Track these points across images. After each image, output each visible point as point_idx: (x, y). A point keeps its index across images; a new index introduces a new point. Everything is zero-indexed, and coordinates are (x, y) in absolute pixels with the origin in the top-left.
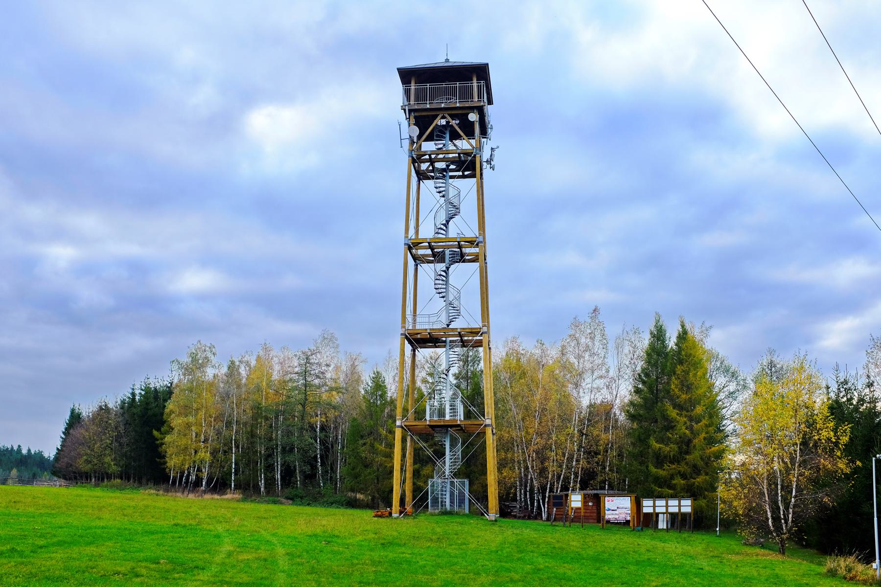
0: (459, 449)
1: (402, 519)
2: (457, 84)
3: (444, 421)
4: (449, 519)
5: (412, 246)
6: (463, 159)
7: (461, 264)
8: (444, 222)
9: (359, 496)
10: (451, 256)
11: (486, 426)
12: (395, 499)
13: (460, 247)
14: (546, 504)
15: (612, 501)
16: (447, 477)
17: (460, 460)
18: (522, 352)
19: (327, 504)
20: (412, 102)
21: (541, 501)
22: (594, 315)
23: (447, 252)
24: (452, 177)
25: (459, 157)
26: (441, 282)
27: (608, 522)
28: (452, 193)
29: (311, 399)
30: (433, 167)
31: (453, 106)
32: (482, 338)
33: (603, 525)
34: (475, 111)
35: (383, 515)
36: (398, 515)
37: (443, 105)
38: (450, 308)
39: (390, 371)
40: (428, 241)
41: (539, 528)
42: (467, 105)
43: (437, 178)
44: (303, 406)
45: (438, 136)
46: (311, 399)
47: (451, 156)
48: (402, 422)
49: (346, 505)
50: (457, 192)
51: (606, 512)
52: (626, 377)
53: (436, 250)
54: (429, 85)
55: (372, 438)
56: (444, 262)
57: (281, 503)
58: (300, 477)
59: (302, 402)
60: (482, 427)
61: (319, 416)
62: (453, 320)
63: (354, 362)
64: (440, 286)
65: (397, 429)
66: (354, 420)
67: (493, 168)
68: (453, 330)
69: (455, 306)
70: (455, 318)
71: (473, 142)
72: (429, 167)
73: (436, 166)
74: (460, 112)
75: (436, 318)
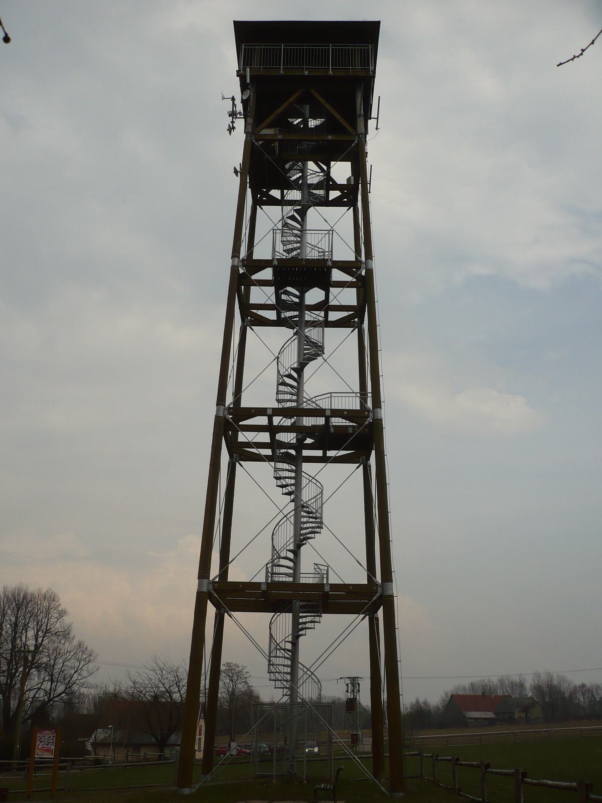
8: (291, 547)
26: (288, 397)
38: (303, 514)
62: (307, 625)
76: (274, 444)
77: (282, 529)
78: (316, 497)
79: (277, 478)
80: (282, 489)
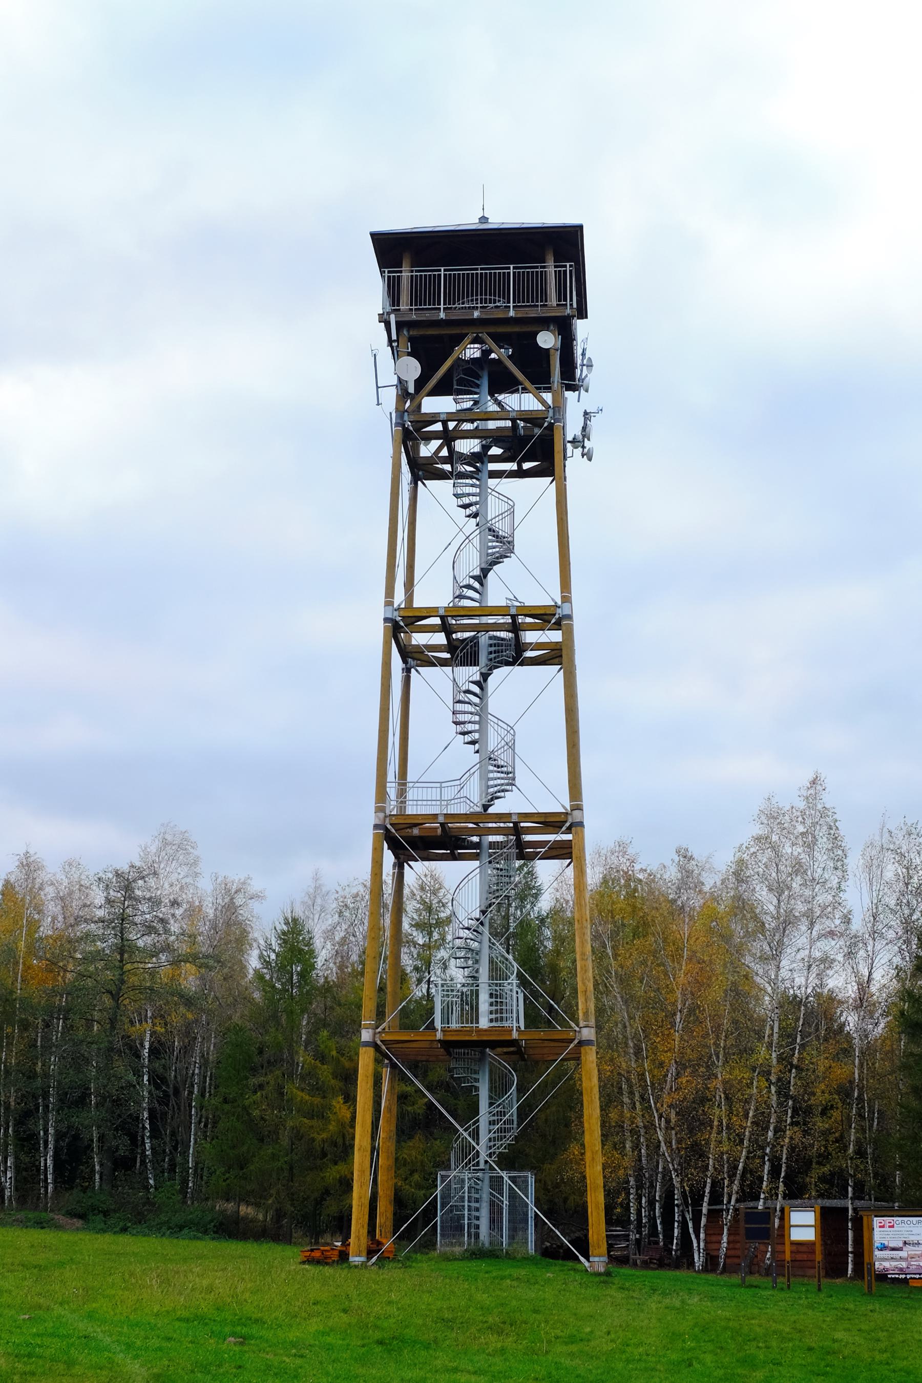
0: (512, 1102)
1: (375, 1268)
2: (509, 268)
3: (479, 1031)
4: (490, 1268)
5: (402, 624)
6: (522, 432)
7: (517, 669)
8: (477, 572)
9: (245, 1210)
10: (493, 649)
11: (581, 1043)
12: (358, 1219)
13: (515, 628)
14: (702, 1231)
15: (890, 1227)
16: (482, 1166)
17: (515, 1126)
18: (641, 876)
19: (169, 1228)
20: (404, 307)
21: (690, 1225)
22: (812, 791)
23: (484, 639)
24: (494, 474)
25: (515, 426)
27: (882, 1277)
28: (494, 507)
29: (133, 980)
30: (451, 450)
31: (501, 316)
32: (569, 837)
33: (870, 1287)
34: (552, 327)
35: (326, 1258)
36: (363, 1259)
37: (476, 314)
38: (491, 768)
39: (316, 920)
40: (442, 612)
41: (724, 1292)
42: (533, 313)
43: (462, 475)
44: (115, 996)
45: (460, 382)
46: (133, 980)
47: (492, 425)
48: (375, 1034)
49: (215, 1232)
50: (506, 507)
51: (877, 1253)
52: (891, 935)
53: (454, 636)
54: (445, 270)
55: (279, 1073)
56: (476, 663)
57: (59, 1227)
58: (101, 1165)
59: (113, 989)
60: (572, 1045)
61: (149, 1021)
62: (499, 794)
63: (232, 899)
64: (467, 717)
65: (362, 1050)
66: (239, 1030)
67: (588, 455)
68: (500, 817)
69: (501, 763)
70: (503, 791)
71: (548, 397)
72: (440, 449)
73: (456, 449)
74: (517, 329)
75: (457, 788)
77: (463, 555)
78: (502, 514)
79: (456, 723)
80: (464, 510)
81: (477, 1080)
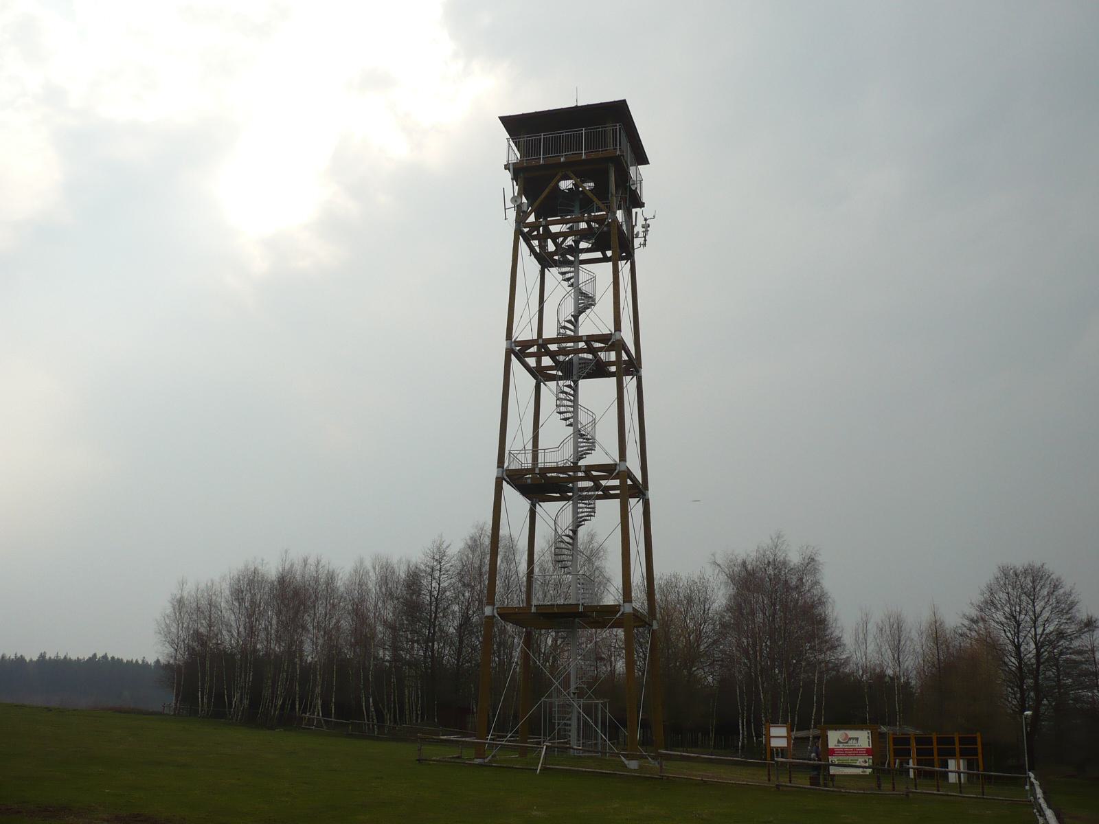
28: (583, 277)
42: (601, 155)
70: (585, 454)
76: (558, 365)
81: (573, 206)
